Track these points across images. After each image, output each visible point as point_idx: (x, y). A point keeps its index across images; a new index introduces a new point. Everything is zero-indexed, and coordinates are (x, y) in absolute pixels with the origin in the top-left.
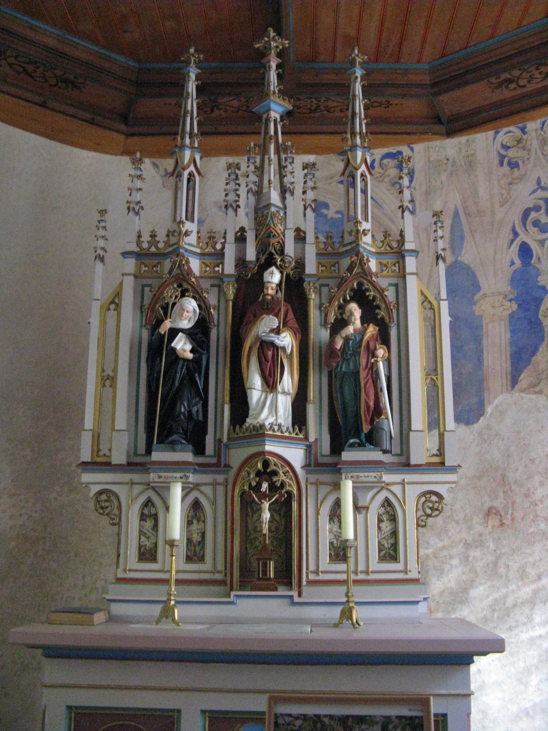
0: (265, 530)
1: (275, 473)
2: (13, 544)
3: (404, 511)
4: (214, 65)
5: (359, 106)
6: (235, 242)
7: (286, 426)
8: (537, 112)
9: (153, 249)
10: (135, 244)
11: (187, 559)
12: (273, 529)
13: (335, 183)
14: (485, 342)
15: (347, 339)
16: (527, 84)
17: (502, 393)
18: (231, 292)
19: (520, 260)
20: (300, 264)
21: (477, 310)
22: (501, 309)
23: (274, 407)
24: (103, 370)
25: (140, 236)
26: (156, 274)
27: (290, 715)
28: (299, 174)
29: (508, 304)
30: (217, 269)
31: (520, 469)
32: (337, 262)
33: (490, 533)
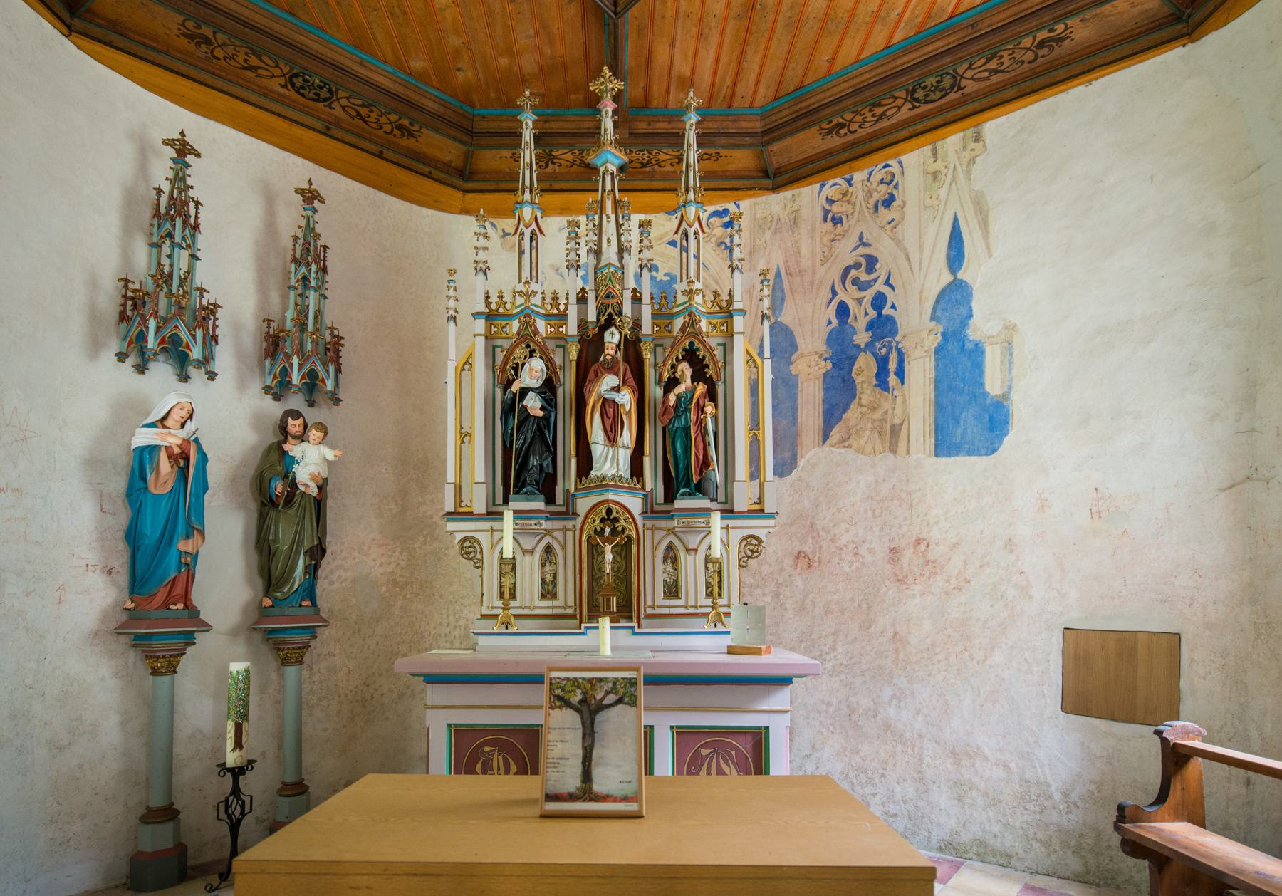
0: (608, 568)
1: (616, 520)
2: (384, 589)
5: (692, 156)
6: (577, 303)
9: (501, 310)
10: (484, 305)
12: (615, 569)
13: (664, 244)
14: (799, 400)
15: (679, 397)
18: (574, 352)
20: (637, 325)
21: (794, 369)
22: (817, 368)
23: (615, 459)
24: (462, 428)
25: (488, 297)
26: (506, 335)
27: (559, 678)
28: (636, 232)
29: (823, 363)
30: (561, 330)
32: (670, 323)
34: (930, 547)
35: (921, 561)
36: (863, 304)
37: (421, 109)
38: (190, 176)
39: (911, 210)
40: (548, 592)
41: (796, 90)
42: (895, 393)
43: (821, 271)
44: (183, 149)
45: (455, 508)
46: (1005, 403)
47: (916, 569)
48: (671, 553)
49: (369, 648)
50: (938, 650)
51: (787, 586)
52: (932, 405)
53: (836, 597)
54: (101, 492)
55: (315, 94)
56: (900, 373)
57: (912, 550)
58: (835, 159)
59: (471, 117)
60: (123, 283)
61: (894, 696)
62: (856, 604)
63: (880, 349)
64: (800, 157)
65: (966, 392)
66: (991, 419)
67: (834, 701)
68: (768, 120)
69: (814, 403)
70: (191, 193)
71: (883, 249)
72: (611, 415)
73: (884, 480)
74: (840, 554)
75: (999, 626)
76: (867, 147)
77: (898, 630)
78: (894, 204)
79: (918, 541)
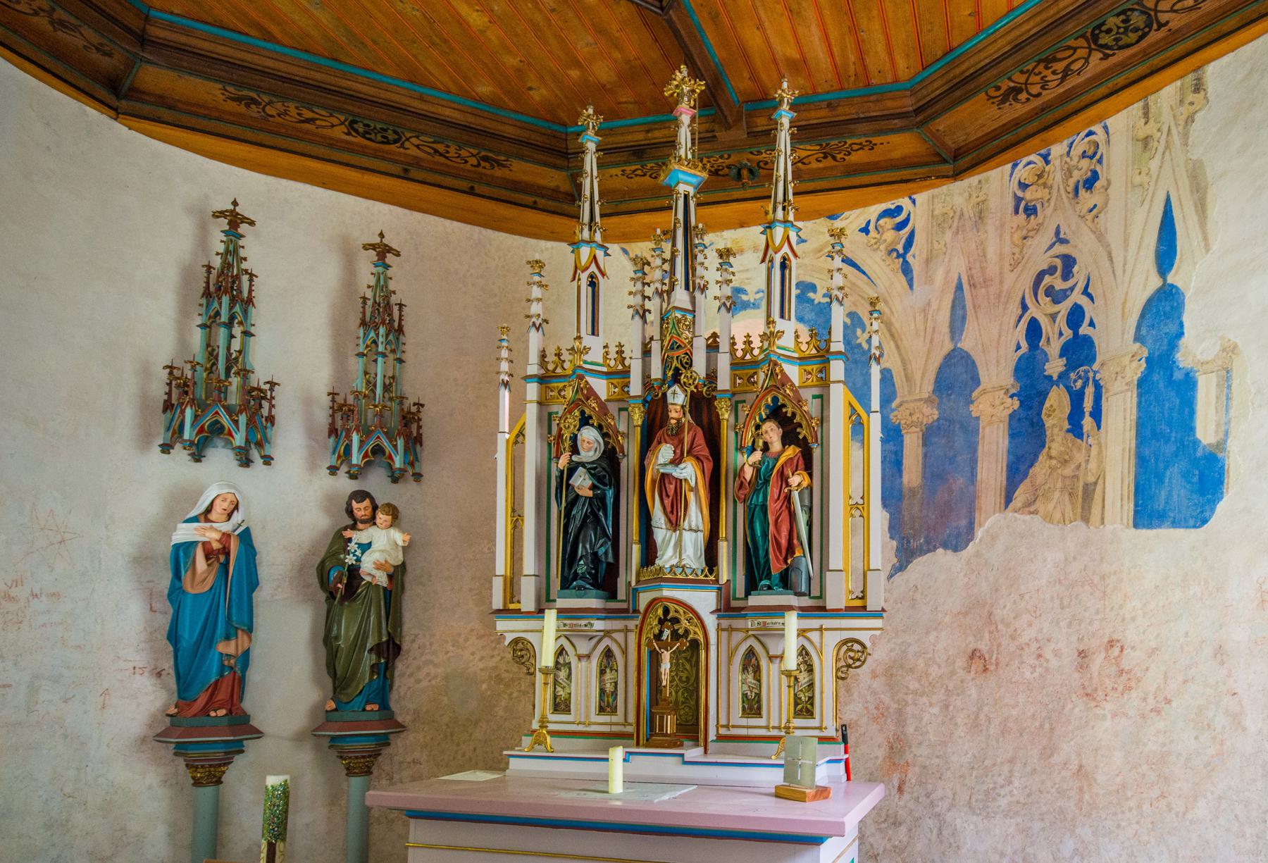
2: (484, 686)
3: (821, 661)
4: (651, 118)
7: (701, 568)
8: (1057, 131)
9: (559, 370)
11: (600, 711)
13: (824, 258)
14: (980, 451)
16: (1041, 91)
17: (994, 514)
18: (638, 418)
19: (1027, 342)
20: (712, 377)
21: (974, 410)
22: (1002, 407)
28: (713, 260)
31: (1009, 606)
33: (973, 679)
34: (1125, 652)
35: (1113, 670)
36: (1057, 322)
37: (503, 138)
38: (243, 247)
39: (1116, 191)
40: (606, 707)
41: (946, 54)
42: (1090, 441)
43: (1010, 278)
44: (235, 220)
45: (505, 604)
46: (1220, 455)
47: (1107, 681)
48: (753, 660)
49: (464, 755)
50: (1129, 794)
51: (958, 695)
52: (1133, 457)
53: (1014, 712)
54: (151, 590)
55: (383, 137)
56: (1097, 414)
57: (1103, 655)
58: (1022, 132)
59: (564, 136)
60: (168, 370)
61: (1076, 850)
62: (1037, 724)
63: (1075, 381)
64: (980, 134)
65: (1173, 439)
66: (1202, 477)
67: (1009, 850)
68: (919, 95)
69: (997, 455)
70: (244, 265)
71: (1083, 247)
72: (671, 493)
73: (1075, 558)
74: (1021, 655)
75: (1205, 767)
76: (1059, 112)
77: (1084, 762)
78: (1097, 184)
79: (1111, 644)
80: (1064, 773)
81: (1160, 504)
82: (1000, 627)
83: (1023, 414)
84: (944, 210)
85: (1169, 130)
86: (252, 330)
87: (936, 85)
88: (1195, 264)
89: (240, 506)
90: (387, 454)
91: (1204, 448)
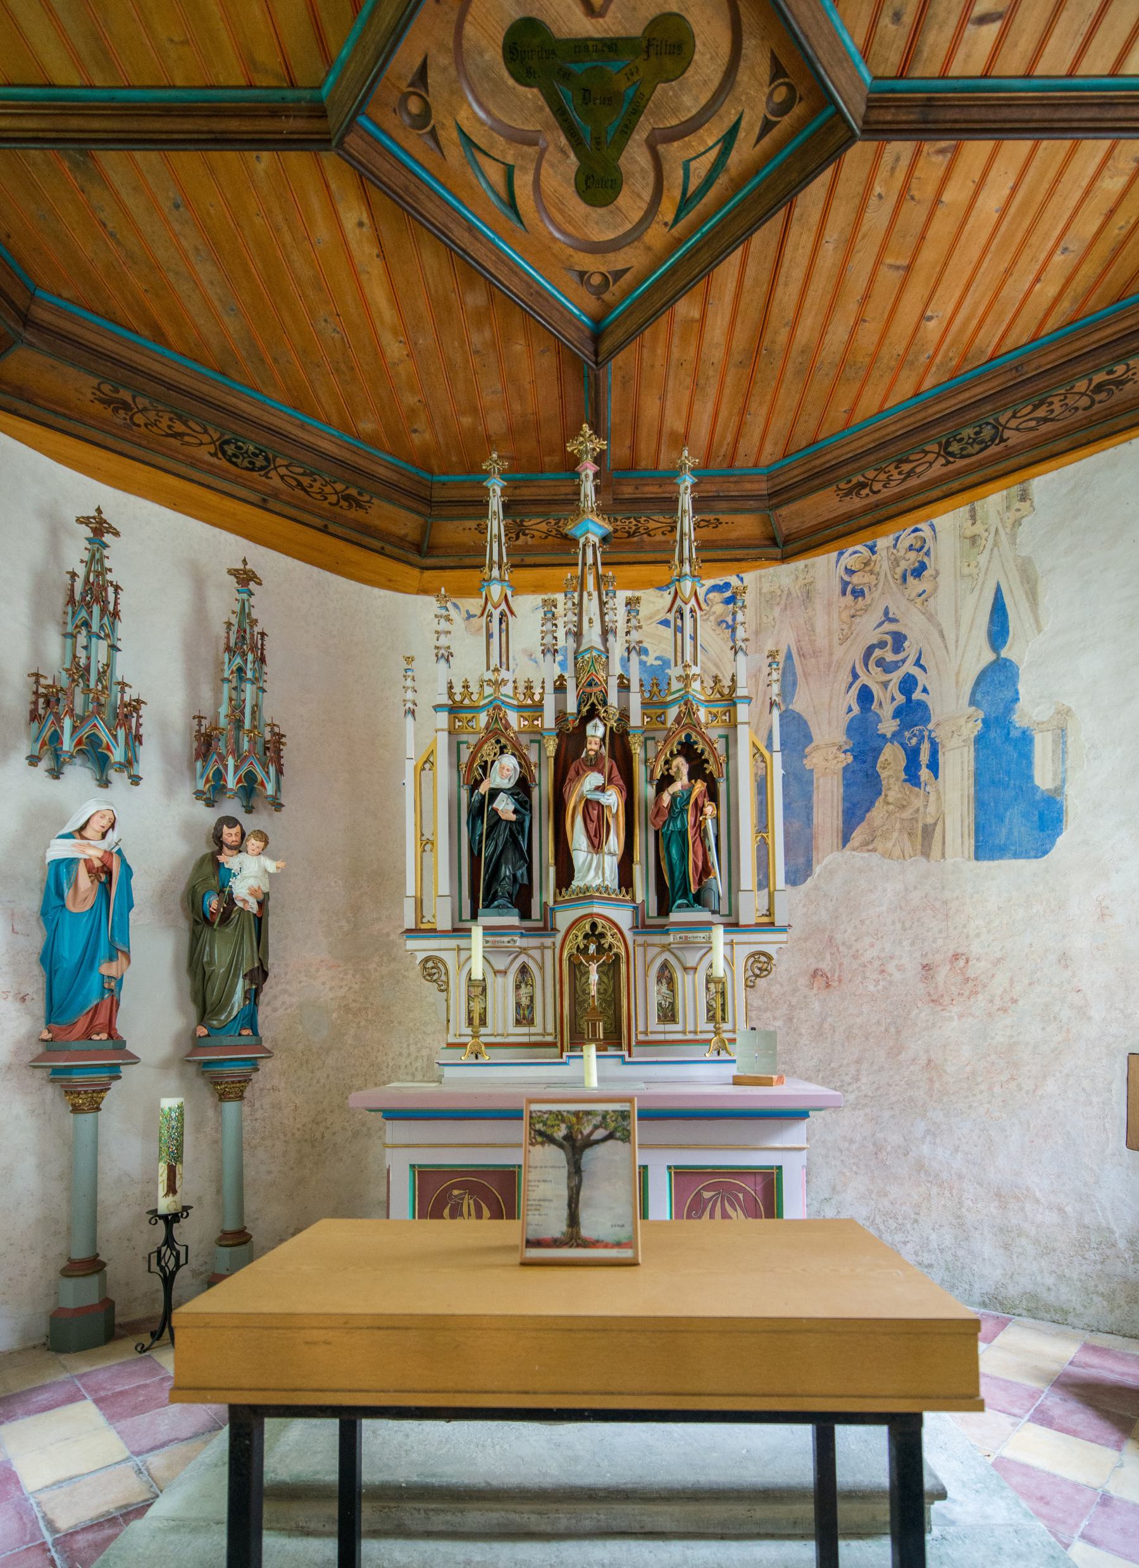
1: (602, 935)
2: (335, 1015)
4: (519, 476)
5: (687, 523)
8: (889, 525)
9: (467, 702)
10: (447, 696)
14: (815, 797)
15: (674, 797)
18: (551, 747)
20: (624, 716)
21: (808, 763)
23: (600, 867)
24: (422, 835)
25: (451, 688)
28: (622, 612)
30: (536, 723)
34: (970, 963)
35: (959, 979)
36: (889, 688)
37: (371, 476)
40: (524, 1017)
42: (928, 789)
46: (1058, 799)
47: (953, 988)
48: (666, 973)
49: (318, 1082)
50: (979, 1079)
51: (802, 1009)
53: (858, 1021)
55: (250, 462)
56: (934, 766)
57: (948, 967)
58: (854, 524)
60: (34, 678)
61: (928, 1131)
62: (883, 1029)
63: (910, 739)
64: (814, 522)
67: (858, 1137)
68: (776, 481)
71: (913, 625)
72: (595, 818)
73: (915, 888)
76: (893, 509)
80: (912, 1068)
81: (1002, 839)
82: (842, 949)
83: (857, 767)
84: (772, 589)
85: (997, 531)
86: (119, 645)
87: (795, 472)
88: (1027, 642)
89: (116, 825)
90: (259, 780)
91: (1043, 792)
